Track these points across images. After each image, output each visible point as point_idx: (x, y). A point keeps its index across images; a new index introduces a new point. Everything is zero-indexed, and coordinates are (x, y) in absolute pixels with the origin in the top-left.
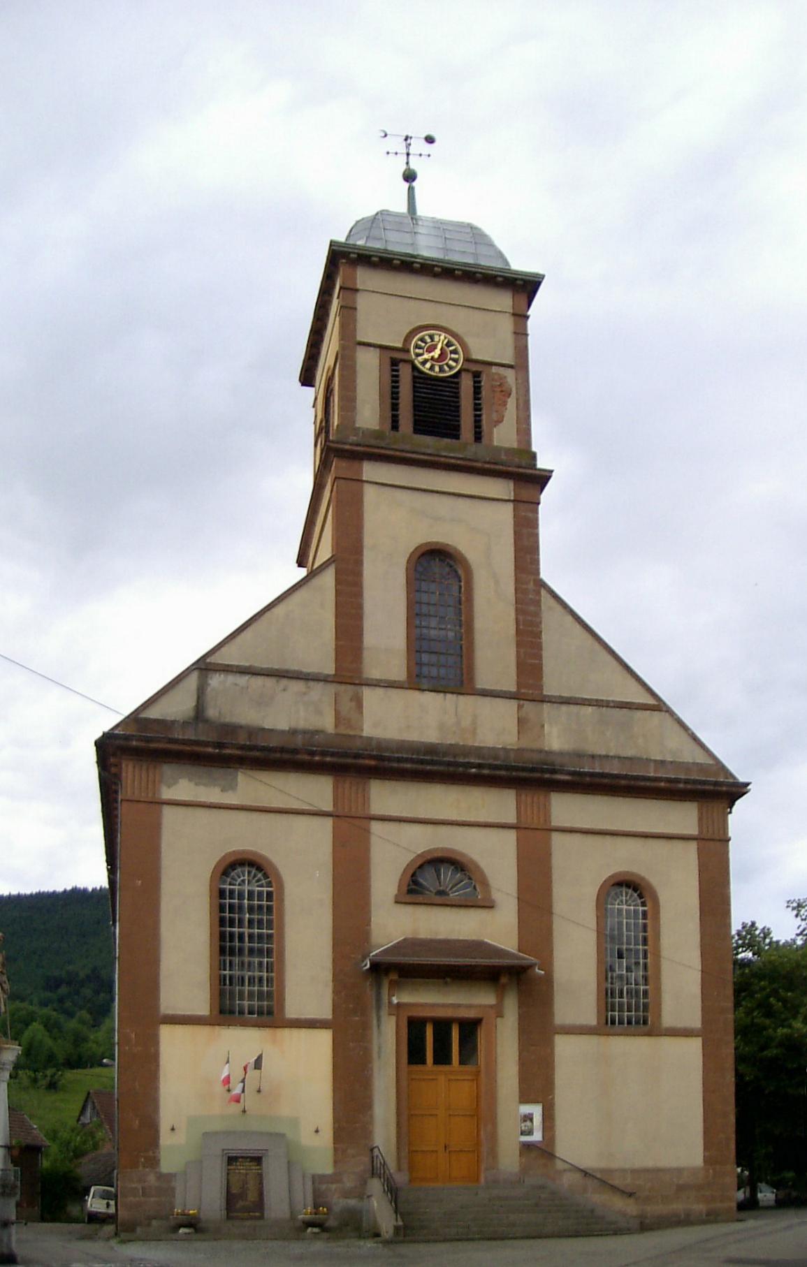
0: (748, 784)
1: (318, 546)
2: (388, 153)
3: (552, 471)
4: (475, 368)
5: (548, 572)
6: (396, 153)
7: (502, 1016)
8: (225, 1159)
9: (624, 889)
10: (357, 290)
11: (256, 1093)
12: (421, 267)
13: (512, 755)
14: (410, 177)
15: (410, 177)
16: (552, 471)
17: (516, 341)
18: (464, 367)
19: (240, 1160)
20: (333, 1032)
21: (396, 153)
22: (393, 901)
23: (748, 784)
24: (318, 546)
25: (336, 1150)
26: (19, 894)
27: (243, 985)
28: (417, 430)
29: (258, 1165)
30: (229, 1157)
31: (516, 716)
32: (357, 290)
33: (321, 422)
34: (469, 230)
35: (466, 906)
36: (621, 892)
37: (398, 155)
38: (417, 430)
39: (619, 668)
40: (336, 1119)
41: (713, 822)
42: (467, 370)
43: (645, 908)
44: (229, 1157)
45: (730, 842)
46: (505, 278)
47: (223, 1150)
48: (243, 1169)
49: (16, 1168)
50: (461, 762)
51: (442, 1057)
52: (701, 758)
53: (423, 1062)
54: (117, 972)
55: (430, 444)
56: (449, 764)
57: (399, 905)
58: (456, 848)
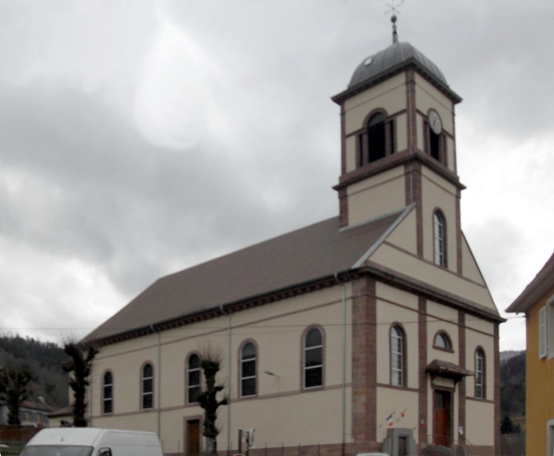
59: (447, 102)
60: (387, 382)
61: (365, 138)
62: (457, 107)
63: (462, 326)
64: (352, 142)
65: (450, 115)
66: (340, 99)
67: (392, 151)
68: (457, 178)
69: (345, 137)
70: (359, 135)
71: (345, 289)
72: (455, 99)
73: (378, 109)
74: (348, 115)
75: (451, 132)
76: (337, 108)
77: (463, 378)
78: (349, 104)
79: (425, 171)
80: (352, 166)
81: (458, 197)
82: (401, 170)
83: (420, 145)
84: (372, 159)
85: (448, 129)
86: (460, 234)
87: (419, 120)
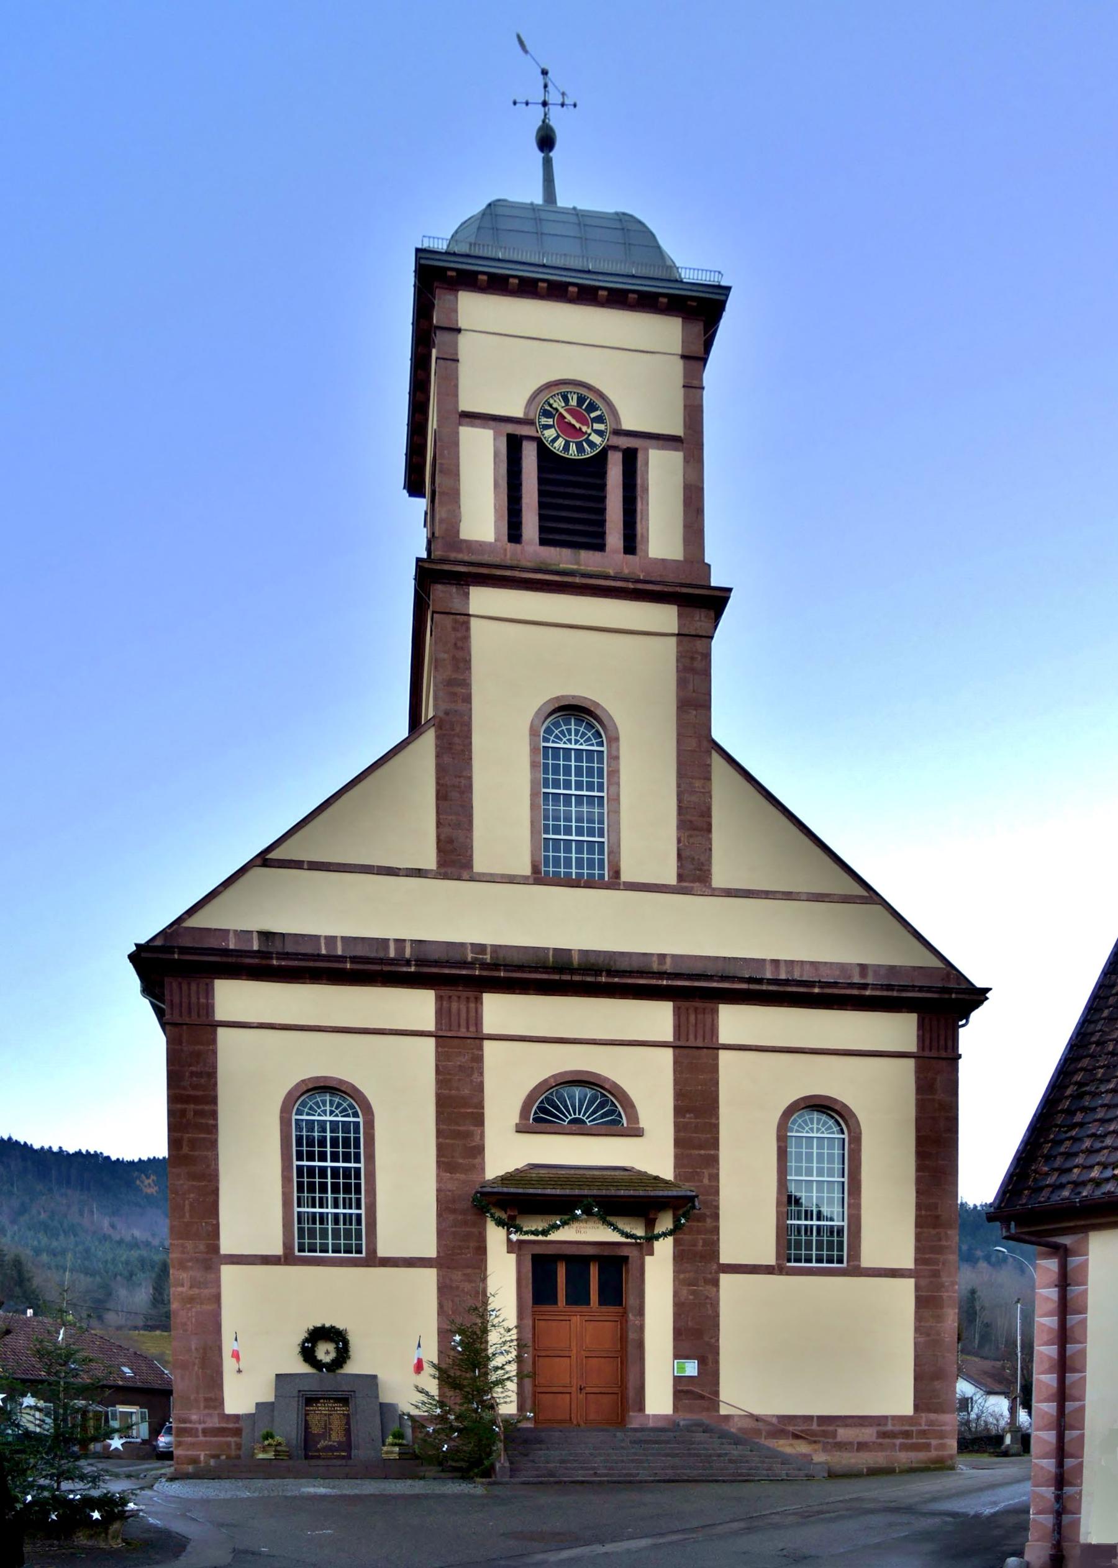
0: (988, 990)
2: (515, 103)
3: (730, 590)
4: (625, 442)
6: (527, 104)
8: (302, 1401)
9: (815, 1115)
10: (459, 331)
12: (520, 284)
13: (601, 959)
14: (546, 141)
15: (546, 141)
16: (730, 590)
17: (686, 397)
18: (610, 443)
19: (322, 1401)
21: (527, 104)
22: (514, 1129)
23: (988, 990)
26: (10, 1139)
27: (314, 1223)
28: (543, 542)
30: (306, 1398)
32: (459, 331)
34: (574, 219)
35: (622, 1136)
37: (530, 105)
38: (543, 542)
41: (938, 1036)
42: (615, 448)
44: (306, 1398)
45: (960, 1061)
47: (299, 1391)
49: (143, 1410)
51: (577, 1296)
53: (554, 1301)
55: (562, 558)
56: (751, 980)
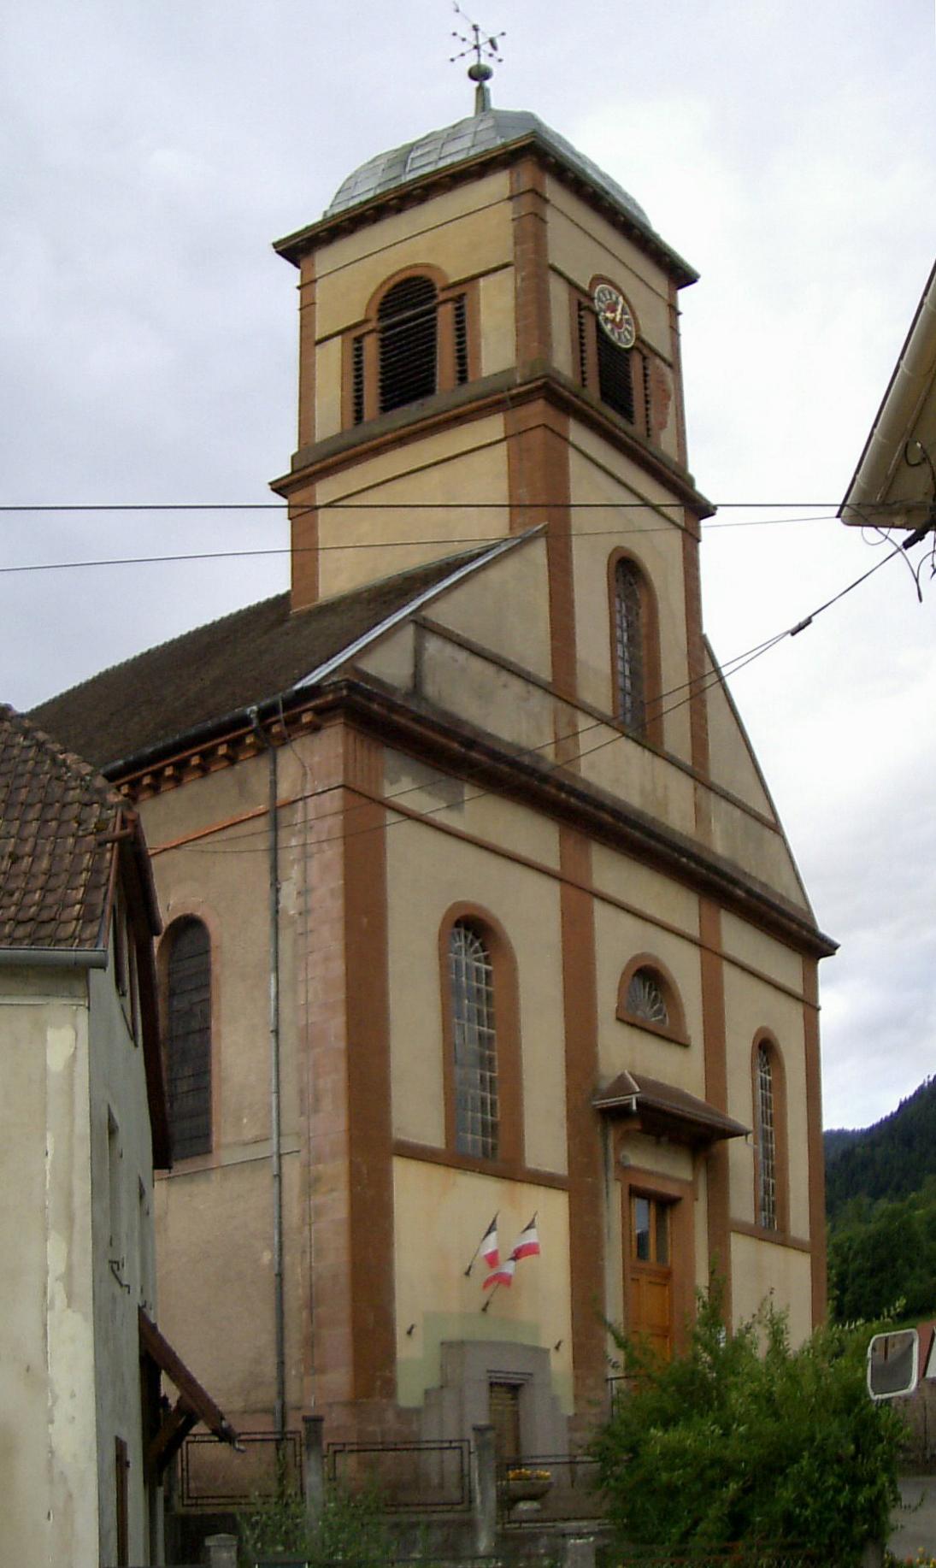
1: (761, 646)
5: (707, 629)
7: (697, 1199)
11: (464, 1276)
20: (570, 1197)
24: (761, 646)
25: (576, 1377)
29: (512, 1399)
31: (692, 800)
33: (663, 425)
36: (459, 933)
39: (753, 770)
40: (575, 1332)
43: (490, 968)
46: (642, 235)
48: (499, 1405)
50: (756, 892)
52: (802, 905)
54: (138, 997)
57: (619, 1024)
58: (660, 957)
59: (659, 282)
60: (714, 674)
61: (371, 347)
62: (685, 296)
63: (712, 954)
64: (332, 358)
65: (664, 312)
66: (296, 249)
67: (462, 378)
68: (690, 481)
69: (309, 342)
70: (354, 336)
71: (291, 747)
72: (680, 275)
73: (611, 556)
74: (320, 292)
75: (666, 353)
76: (291, 275)
77: (716, 1147)
78: (325, 260)
79: (578, 434)
80: (330, 421)
81: (691, 538)
82: (492, 427)
83: (562, 360)
84: (394, 398)
85: (656, 338)
86: (698, 648)
87: (558, 293)
